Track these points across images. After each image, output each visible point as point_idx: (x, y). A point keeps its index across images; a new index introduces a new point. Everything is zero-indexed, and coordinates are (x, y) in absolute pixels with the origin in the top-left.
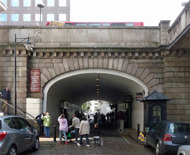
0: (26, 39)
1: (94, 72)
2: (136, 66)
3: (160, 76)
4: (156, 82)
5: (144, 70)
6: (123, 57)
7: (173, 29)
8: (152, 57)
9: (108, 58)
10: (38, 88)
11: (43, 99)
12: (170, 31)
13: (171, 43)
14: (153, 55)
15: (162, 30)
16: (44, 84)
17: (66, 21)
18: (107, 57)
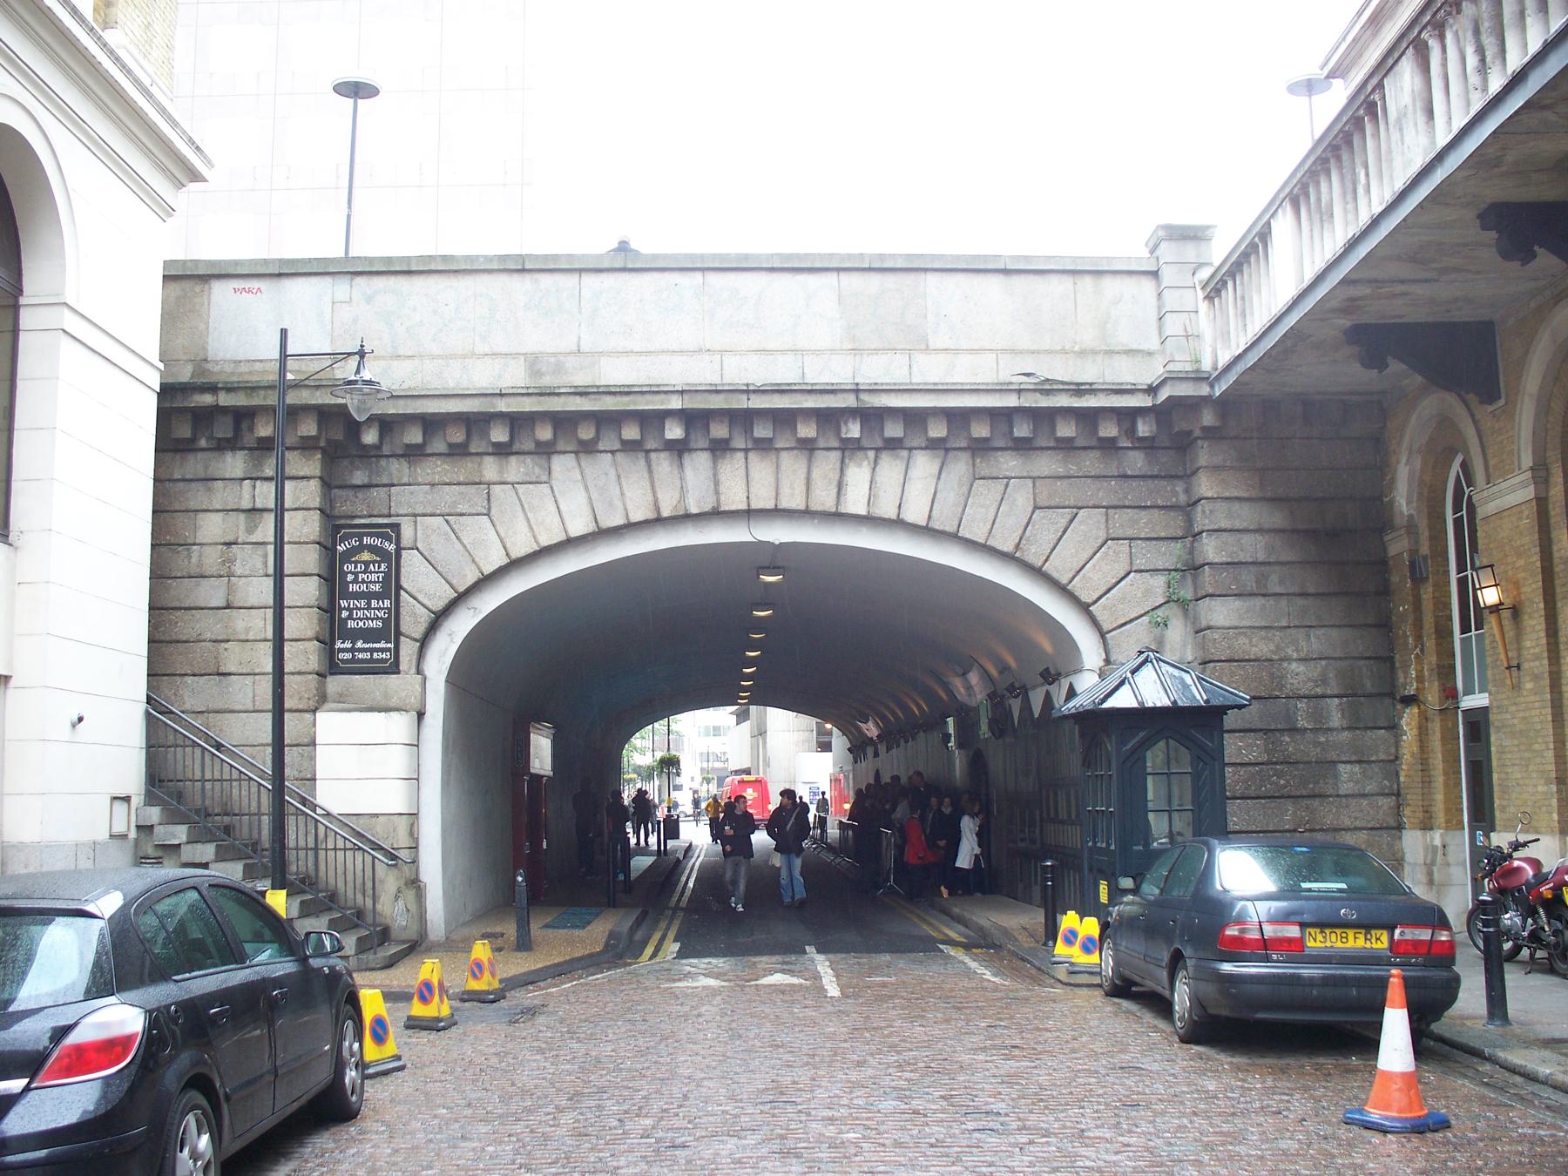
0: (349, 354)
1: (751, 539)
2: (1021, 497)
3: (1169, 555)
4: (1148, 592)
5: (1071, 521)
6: (934, 445)
7: (1230, 284)
8: (986, 440)
9: (843, 450)
10: (382, 645)
11: (421, 715)
12: (1214, 291)
13: (1228, 368)
14: (555, 434)
15: (1168, 276)
16: (425, 618)
17: (397, 726)
18: (836, 444)
